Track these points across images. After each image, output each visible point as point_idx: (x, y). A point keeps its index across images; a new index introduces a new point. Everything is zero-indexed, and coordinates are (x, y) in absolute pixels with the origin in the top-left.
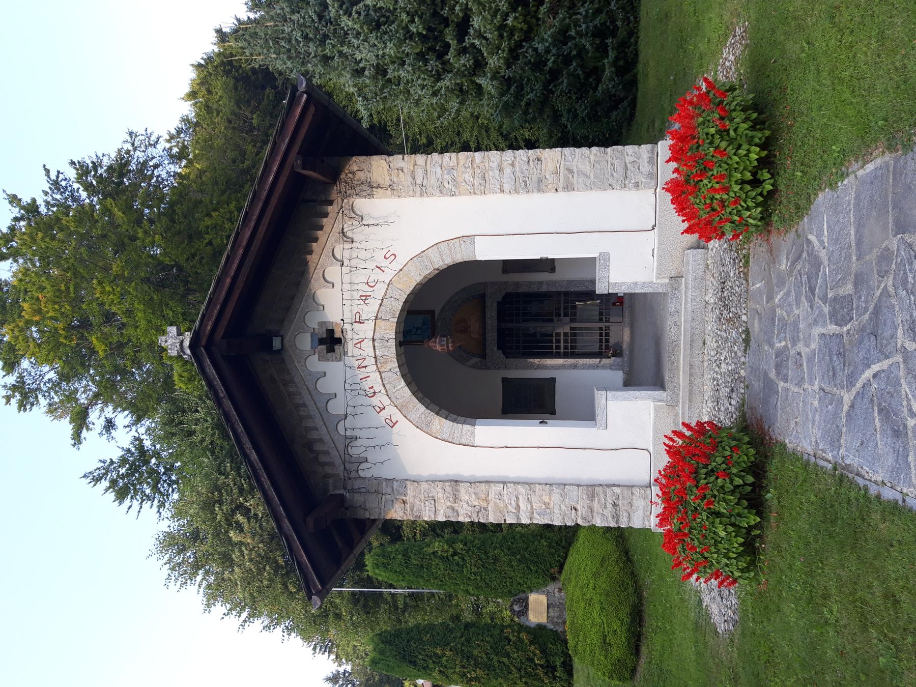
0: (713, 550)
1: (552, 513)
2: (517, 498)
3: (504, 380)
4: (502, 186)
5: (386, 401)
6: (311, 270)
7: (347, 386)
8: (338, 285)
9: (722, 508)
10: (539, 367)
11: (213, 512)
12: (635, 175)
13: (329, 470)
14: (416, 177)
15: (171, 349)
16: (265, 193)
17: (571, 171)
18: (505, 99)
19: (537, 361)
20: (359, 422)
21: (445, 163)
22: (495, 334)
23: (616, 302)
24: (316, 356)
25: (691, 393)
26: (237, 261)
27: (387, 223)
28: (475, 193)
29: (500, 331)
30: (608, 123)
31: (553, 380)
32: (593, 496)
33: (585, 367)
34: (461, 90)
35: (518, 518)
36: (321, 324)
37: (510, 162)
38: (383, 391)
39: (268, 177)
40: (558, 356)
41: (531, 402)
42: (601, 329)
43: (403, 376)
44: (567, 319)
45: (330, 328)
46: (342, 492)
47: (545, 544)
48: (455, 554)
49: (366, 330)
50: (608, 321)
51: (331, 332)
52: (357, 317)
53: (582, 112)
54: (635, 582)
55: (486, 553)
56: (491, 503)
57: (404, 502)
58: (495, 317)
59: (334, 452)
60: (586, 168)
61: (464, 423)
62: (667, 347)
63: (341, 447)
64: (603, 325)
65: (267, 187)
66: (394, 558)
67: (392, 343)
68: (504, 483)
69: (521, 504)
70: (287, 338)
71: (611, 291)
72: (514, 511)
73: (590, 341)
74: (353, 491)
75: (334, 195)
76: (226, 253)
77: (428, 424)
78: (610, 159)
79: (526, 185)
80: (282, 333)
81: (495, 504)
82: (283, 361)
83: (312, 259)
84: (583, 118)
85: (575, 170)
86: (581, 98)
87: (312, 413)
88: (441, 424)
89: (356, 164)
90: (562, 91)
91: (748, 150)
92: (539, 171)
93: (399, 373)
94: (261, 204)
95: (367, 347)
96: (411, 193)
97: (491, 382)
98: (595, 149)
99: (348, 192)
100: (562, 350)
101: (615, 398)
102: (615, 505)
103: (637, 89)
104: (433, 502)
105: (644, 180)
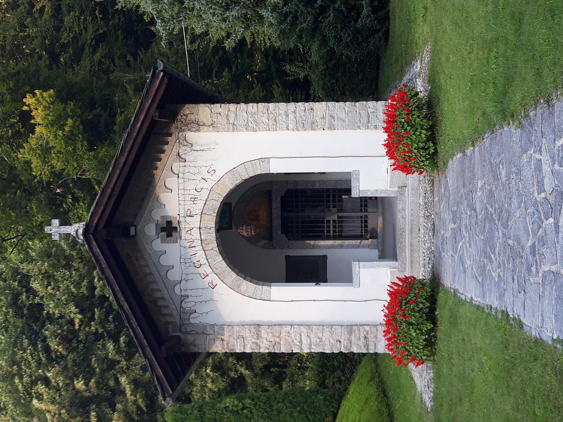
0: (410, 344)
1: (324, 345)
2: (301, 335)
3: (287, 257)
4: (288, 126)
5: (209, 271)
6: (157, 180)
7: (182, 260)
8: (175, 191)
9: (413, 320)
10: (314, 247)
11: (13, 384)
12: (374, 121)
13: (169, 319)
14: (230, 119)
15: (54, 235)
16: (135, 134)
17: (333, 117)
18: (283, 27)
19: (312, 242)
20: (190, 285)
21: (249, 110)
22: (280, 221)
23: (366, 202)
24: (159, 239)
25: (412, 262)
26: (115, 178)
27: (209, 149)
28: (269, 130)
29: (283, 219)
30: (367, 46)
31: (325, 257)
32: (351, 332)
33: (349, 247)
34: (246, 18)
35: (301, 349)
36: (163, 217)
37: (293, 110)
38: (207, 264)
39: (137, 124)
40: (328, 238)
41: (310, 271)
42: (361, 217)
43: (220, 253)
44: (335, 210)
45: (170, 220)
46: (178, 334)
47: (321, 397)
48: (244, 408)
49: (195, 222)
50: (366, 211)
51: (169, 223)
52: (189, 213)
53: (346, 37)
54: (389, 410)
55: (271, 406)
56: (283, 339)
57: (222, 340)
58: (279, 208)
59: (172, 307)
60: (343, 115)
61: (263, 285)
62: (398, 233)
63: (177, 303)
64: (362, 214)
65: (136, 130)
66: (190, 414)
67: (213, 230)
68: (291, 325)
69: (303, 339)
70: (139, 227)
71: (360, 196)
72: (298, 344)
73: (354, 226)
74: (186, 333)
75: (173, 130)
76: (109, 173)
77: (239, 286)
78: (358, 110)
79: (304, 126)
80: (135, 223)
81: (286, 339)
82: (136, 244)
83: (157, 173)
84: (347, 43)
85: (336, 117)
86: (345, 27)
87: (156, 279)
88: (247, 286)
89: (188, 109)
90: (329, 22)
91: (421, 132)
92: (312, 117)
93: (218, 251)
94: (132, 141)
95: (196, 234)
96: (226, 129)
97: (278, 258)
98: (348, 103)
99: (183, 128)
100: (332, 234)
101: (365, 267)
102: (365, 338)
103: (389, 23)
104: (242, 339)
105: (380, 124)
